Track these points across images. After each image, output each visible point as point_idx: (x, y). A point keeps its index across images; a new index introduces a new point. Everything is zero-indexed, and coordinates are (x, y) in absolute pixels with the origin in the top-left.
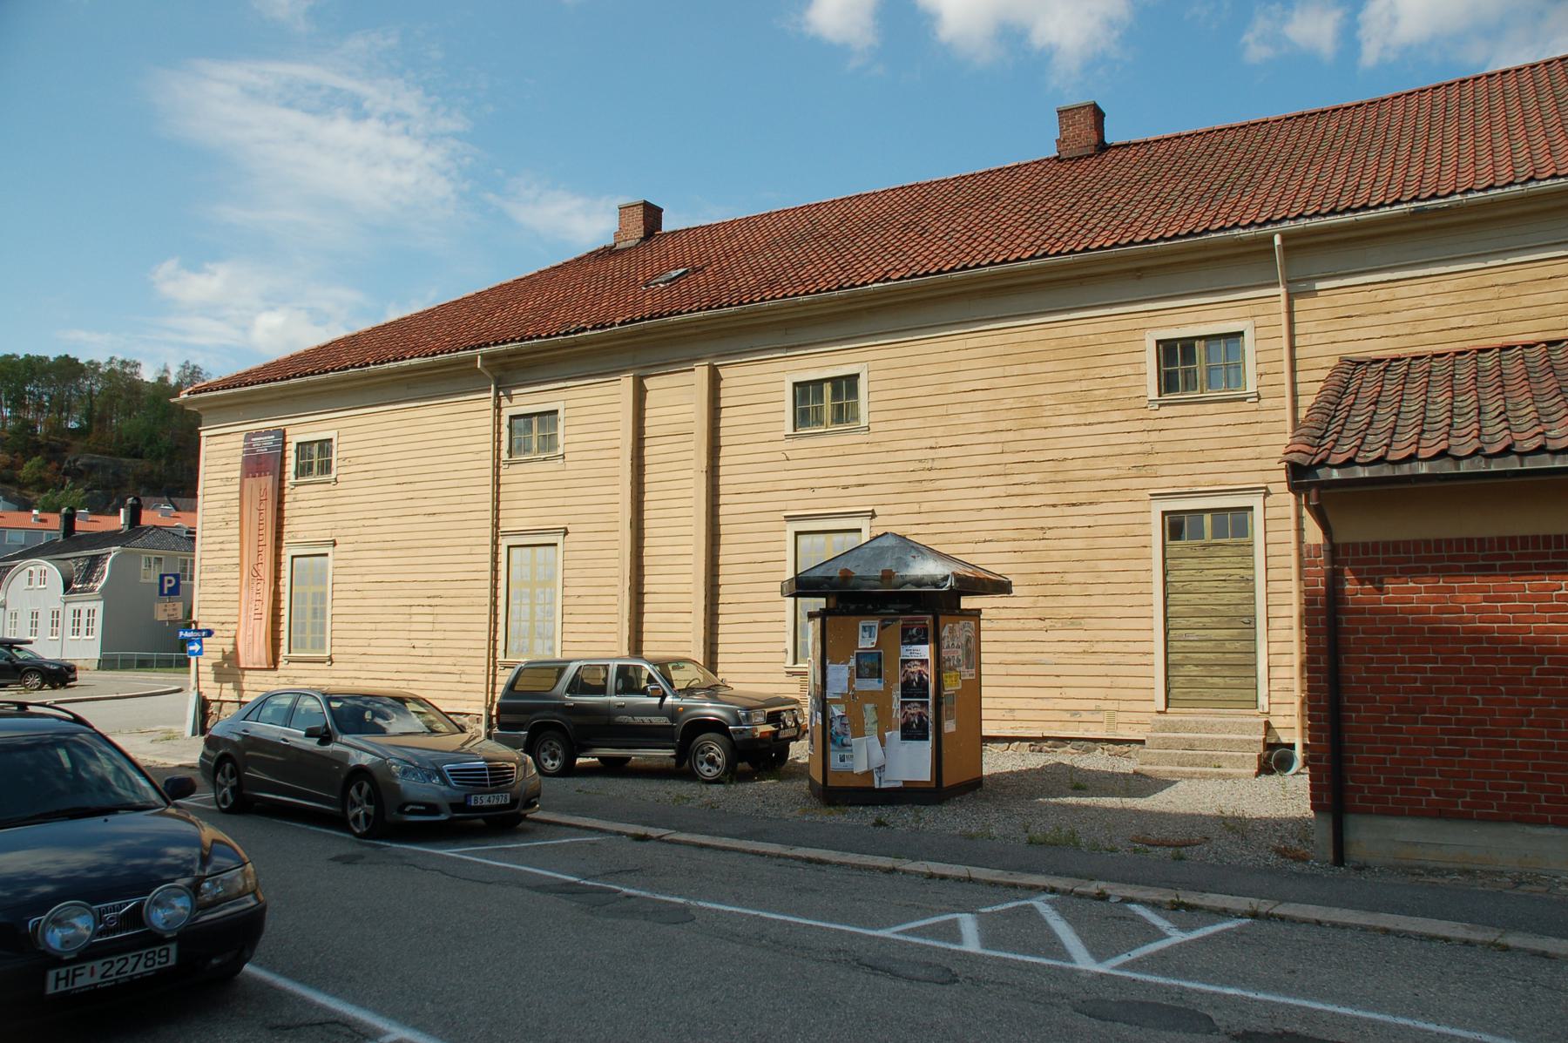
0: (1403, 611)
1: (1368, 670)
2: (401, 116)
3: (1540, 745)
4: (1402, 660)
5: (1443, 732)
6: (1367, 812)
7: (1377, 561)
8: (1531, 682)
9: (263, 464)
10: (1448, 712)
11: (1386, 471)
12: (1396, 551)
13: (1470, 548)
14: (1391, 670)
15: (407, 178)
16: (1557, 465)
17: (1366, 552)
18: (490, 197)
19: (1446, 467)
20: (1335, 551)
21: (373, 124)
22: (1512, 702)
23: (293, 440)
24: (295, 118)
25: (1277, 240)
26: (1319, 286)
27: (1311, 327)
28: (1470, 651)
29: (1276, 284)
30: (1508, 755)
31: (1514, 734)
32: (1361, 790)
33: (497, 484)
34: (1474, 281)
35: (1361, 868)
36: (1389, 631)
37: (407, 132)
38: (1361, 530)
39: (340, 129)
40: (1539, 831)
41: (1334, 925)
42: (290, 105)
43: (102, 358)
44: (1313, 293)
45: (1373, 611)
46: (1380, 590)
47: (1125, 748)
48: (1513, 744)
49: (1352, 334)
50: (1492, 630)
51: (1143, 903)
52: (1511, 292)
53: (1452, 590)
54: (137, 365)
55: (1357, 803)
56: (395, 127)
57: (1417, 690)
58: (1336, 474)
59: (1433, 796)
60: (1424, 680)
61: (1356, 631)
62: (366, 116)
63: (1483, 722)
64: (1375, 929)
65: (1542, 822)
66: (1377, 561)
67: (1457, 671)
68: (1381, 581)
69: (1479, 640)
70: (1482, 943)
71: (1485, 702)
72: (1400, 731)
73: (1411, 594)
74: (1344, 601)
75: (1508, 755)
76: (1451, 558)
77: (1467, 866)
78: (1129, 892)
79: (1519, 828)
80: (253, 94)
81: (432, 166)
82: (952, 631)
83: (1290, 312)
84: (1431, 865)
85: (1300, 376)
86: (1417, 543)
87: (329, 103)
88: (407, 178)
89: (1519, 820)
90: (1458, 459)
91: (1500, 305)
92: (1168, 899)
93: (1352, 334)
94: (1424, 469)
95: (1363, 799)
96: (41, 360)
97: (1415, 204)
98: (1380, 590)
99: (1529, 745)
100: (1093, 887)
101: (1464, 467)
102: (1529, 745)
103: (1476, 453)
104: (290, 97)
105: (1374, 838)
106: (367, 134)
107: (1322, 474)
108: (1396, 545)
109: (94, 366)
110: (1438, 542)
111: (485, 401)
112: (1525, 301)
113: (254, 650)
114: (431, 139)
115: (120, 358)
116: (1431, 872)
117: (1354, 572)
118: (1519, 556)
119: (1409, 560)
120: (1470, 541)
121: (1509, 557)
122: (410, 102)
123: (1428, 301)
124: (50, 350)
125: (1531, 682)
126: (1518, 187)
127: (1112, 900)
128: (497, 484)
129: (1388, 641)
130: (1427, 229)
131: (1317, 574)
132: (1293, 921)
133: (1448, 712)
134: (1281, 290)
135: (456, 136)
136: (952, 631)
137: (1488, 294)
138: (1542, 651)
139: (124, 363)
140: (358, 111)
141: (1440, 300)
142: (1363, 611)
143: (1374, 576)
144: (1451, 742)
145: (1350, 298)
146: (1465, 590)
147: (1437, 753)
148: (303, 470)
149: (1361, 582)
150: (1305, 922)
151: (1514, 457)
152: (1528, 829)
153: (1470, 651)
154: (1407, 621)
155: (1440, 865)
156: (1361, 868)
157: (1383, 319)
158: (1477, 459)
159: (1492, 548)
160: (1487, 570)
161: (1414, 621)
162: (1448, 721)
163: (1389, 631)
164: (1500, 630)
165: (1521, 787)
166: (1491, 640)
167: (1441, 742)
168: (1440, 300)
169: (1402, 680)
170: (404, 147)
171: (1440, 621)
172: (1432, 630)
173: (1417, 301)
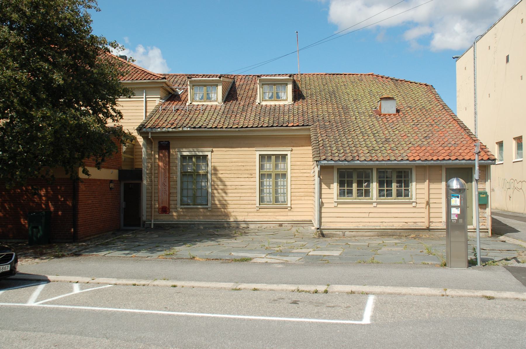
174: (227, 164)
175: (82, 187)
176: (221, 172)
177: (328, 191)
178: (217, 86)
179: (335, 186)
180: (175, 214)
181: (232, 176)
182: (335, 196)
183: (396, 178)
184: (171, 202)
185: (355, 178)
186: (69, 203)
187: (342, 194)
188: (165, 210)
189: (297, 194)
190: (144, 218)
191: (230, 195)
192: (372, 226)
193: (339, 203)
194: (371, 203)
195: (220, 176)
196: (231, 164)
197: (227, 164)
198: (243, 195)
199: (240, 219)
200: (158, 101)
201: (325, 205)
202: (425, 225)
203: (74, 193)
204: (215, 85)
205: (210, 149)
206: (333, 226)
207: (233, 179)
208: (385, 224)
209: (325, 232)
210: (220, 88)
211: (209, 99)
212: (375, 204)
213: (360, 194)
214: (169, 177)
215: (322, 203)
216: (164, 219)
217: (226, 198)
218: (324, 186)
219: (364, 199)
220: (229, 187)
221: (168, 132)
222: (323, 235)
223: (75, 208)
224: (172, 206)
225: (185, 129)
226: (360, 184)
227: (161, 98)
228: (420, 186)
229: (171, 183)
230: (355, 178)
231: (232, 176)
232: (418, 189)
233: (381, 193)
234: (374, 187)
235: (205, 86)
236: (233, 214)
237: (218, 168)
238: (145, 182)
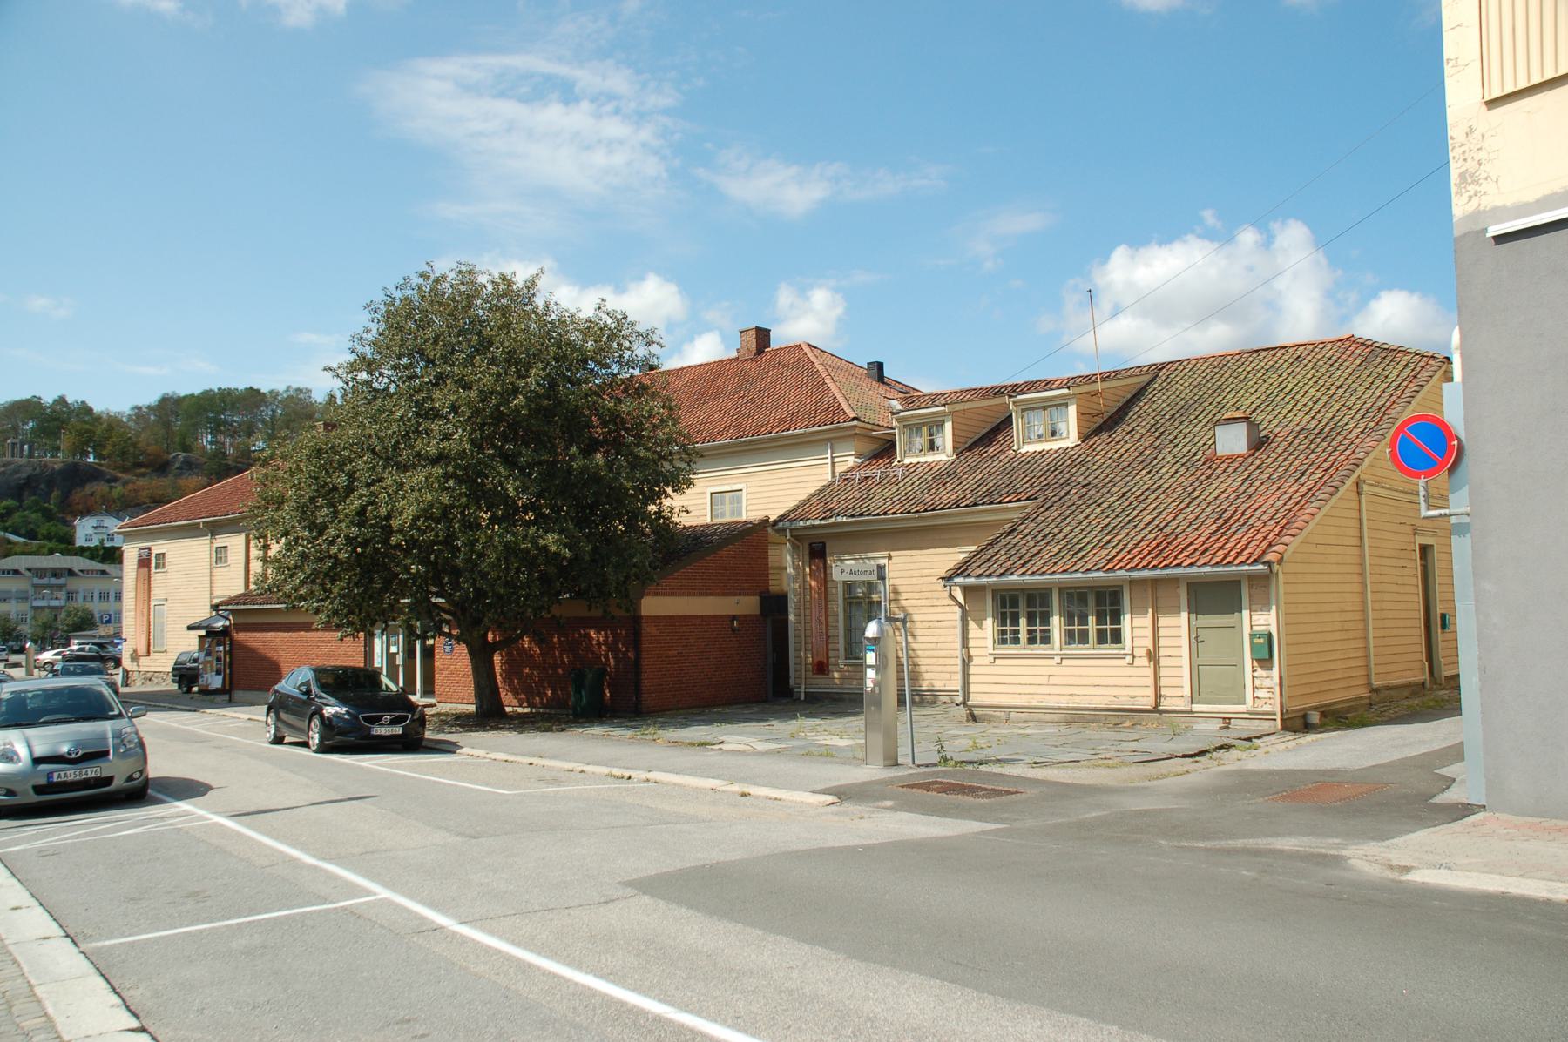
2: (612, 97)
9: (144, 563)
15: (619, 159)
18: (701, 172)
21: (585, 105)
23: (155, 551)
24: (509, 109)
33: (211, 576)
37: (617, 112)
39: (553, 115)
42: (502, 95)
43: (281, 388)
54: (309, 391)
56: (609, 107)
62: (577, 100)
80: (469, 89)
81: (644, 145)
87: (542, 89)
88: (619, 159)
96: (229, 392)
100: (627, 774)
104: (504, 87)
106: (578, 118)
109: (274, 394)
111: (206, 541)
113: (142, 650)
114: (640, 117)
115: (295, 386)
122: (620, 82)
124: (239, 383)
128: (211, 576)
135: (666, 112)
139: (299, 390)
140: (568, 94)
148: (157, 567)
170: (614, 128)
174: (914, 581)
175: (649, 630)
176: (904, 596)
177: (979, 633)
178: (1067, 405)
179: (989, 623)
180: (836, 675)
181: (924, 602)
182: (990, 642)
183: (1097, 610)
184: (831, 654)
185: (1022, 608)
186: (631, 655)
187: (1002, 638)
188: (822, 668)
189: (1408, 623)
190: (792, 682)
191: (920, 639)
192: (1052, 702)
193: (996, 657)
194: (1051, 657)
195: (904, 603)
196: (921, 581)
197: (914, 581)
198: (942, 639)
199: (938, 685)
200: (852, 461)
201: (976, 661)
202: (1148, 703)
203: (635, 639)
204: (1061, 403)
205: (885, 554)
206: (987, 700)
207: (924, 610)
208: (1077, 699)
209: (977, 711)
210: (1072, 410)
211: (932, 447)
212: (1057, 659)
213: (1101, 638)
214: (827, 609)
215: (969, 657)
216: (820, 684)
217: (915, 646)
218: (972, 624)
219: (1039, 649)
220: (918, 625)
221: (813, 527)
222: (973, 718)
223: (637, 663)
224: (832, 660)
225: (840, 519)
226: (1031, 620)
227: (857, 456)
228: (1138, 621)
229: (831, 619)
230: (1022, 608)
231: (924, 602)
232: (1135, 626)
233: (1070, 637)
234: (1056, 623)
235: (1044, 408)
236: (926, 676)
237: (901, 589)
238: (791, 617)
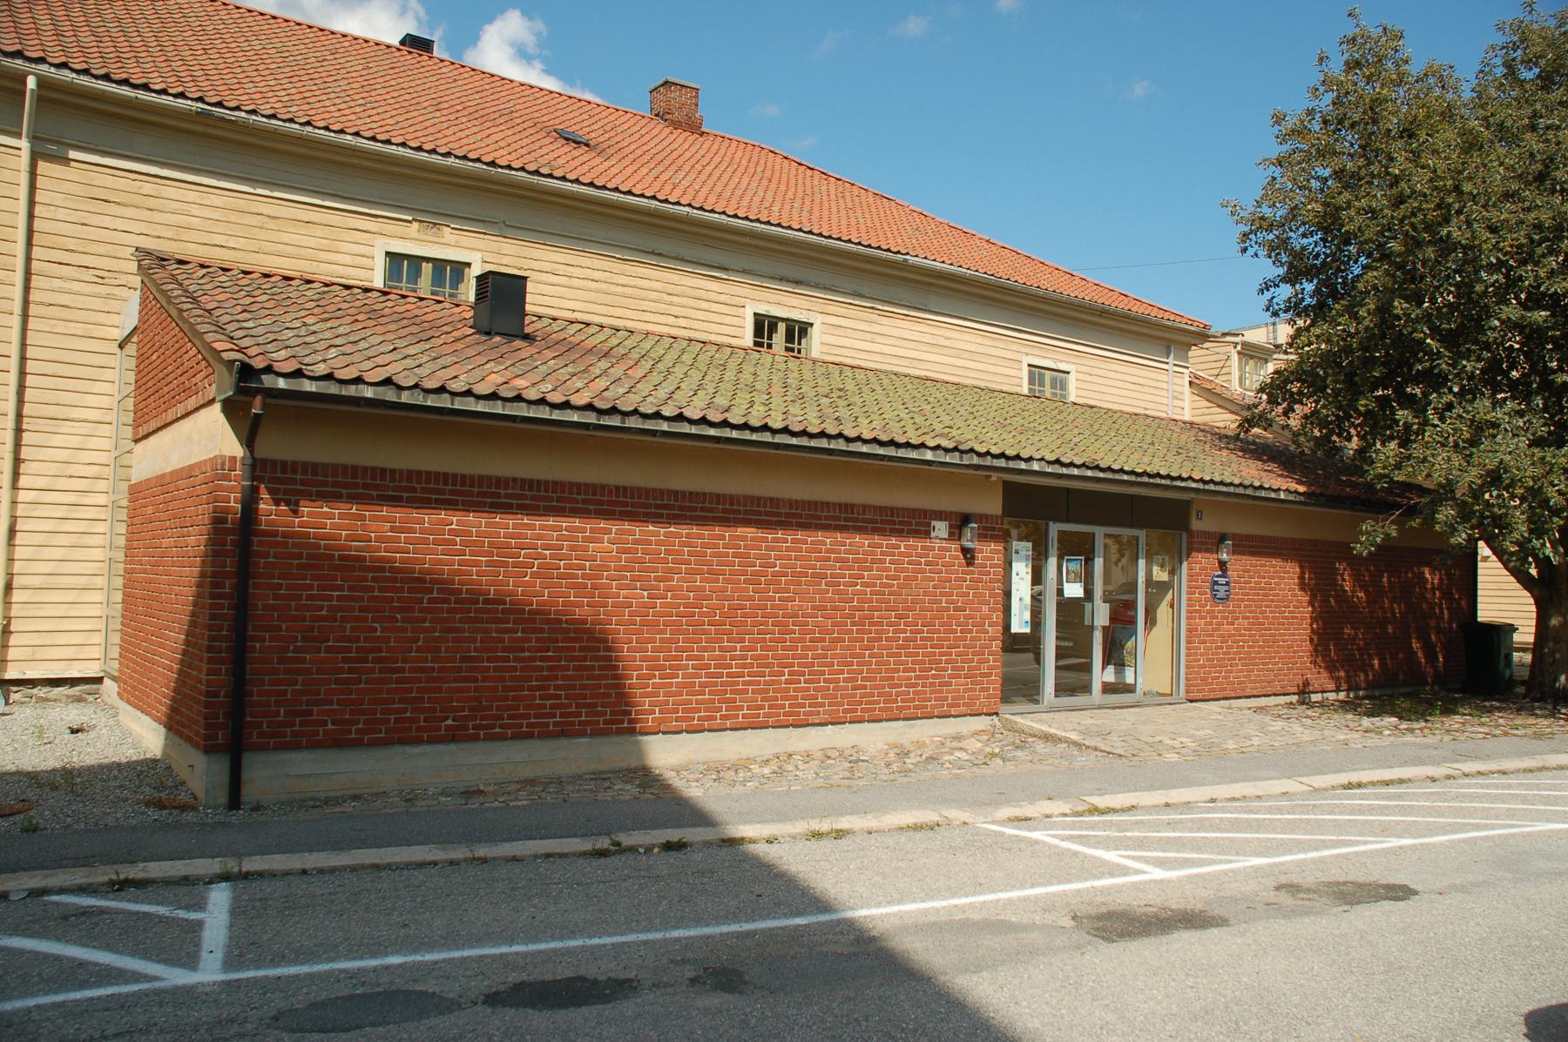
0: (316, 536)
1: (276, 597)
3: (423, 670)
4: (311, 587)
5: (345, 660)
6: (264, 748)
7: (294, 481)
8: (422, 610)
10: (350, 640)
11: (333, 389)
12: (305, 472)
13: (383, 478)
14: (299, 597)
16: (479, 409)
17: (284, 471)
19: (389, 395)
20: (259, 469)
22: (405, 630)
25: (31, 83)
26: (73, 154)
27: (58, 199)
28: (374, 579)
29: (18, 135)
30: (398, 681)
31: (404, 660)
32: (260, 725)
34: (241, 203)
35: (257, 808)
36: (300, 556)
38: (281, 446)
40: (415, 750)
41: (321, 871)
44: (66, 161)
45: (286, 535)
46: (295, 512)
47: (76, 690)
48: (403, 670)
49: (107, 221)
50: (393, 560)
51: (62, 891)
52: (272, 224)
53: (363, 518)
55: (255, 739)
57: (323, 618)
58: (282, 383)
59: (330, 726)
60: (331, 608)
61: (267, 555)
63: (380, 650)
64: (363, 867)
65: (417, 741)
66: (294, 481)
67: (362, 599)
68: (297, 504)
69: (382, 569)
70: (465, 860)
71: (384, 629)
72: (303, 660)
73: (326, 520)
74: (257, 521)
75: (398, 681)
76: (366, 486)
77: (357, 792)
78: (35, 881)
79: (398, 749)
82: (996, 552)
83: (33, 174)
84: (322, 795)
85: (37, 252)
86: (335, 467)
89: (403, 742)
90: (400, 388)
91: (262, 235)
92: (106, 879)
93: (107, 221)
94: (369, 393)
95: (260, 735)
97: (200, 105)
98: (295, 512)
99: (416, 670)
101: (405, 398)
102: (416, 670)
103: (416, 386)
105: (268, 775)
107: (268, 380)
108: (315, 466)
110: (355, 468)
112: (285, 238)
116: (327, 801)
117: (270, 491)
118: (424, 490)
119: (325, 484)
120: (383, 470)
121: (414, 490)
123: (195, 210)
125: (422, 610)
126: (243, 114)
127: (13, 897)
129: (300, 567)
130: (203, 135)
131: (231, 490)
132: (273, 875)
133: (350, 640)
134: (24, 144)
136: (996, 552)
137: (254, 220)
138: (434, 581)
141: (206, 213)
142: (275, 533)
143: (289, 497)
144: (351, 671)
145: (109, 181)
146: (373, 519)
147: (337, 681)
149: (277, 503)
150: (287, 874)
151: (447, 396)
152: (407, 749)
153: (374, 579)
154: (319, 547)
155: (332, 794)
156: (257, 808)
157: (146, 215)
158: (416, 391)
159: (401, 480)
160: (394, 501)
161: (327, 547)
162: (349, 650)
163: (300, 556)
164: (402, 560)
165: (406, 710)
166: (393, 570)
167: (341, 671)
168: (206, 213)
169: (309, 608)
171: (350, 548)
172: (342, 558)
173: (184, 206)
